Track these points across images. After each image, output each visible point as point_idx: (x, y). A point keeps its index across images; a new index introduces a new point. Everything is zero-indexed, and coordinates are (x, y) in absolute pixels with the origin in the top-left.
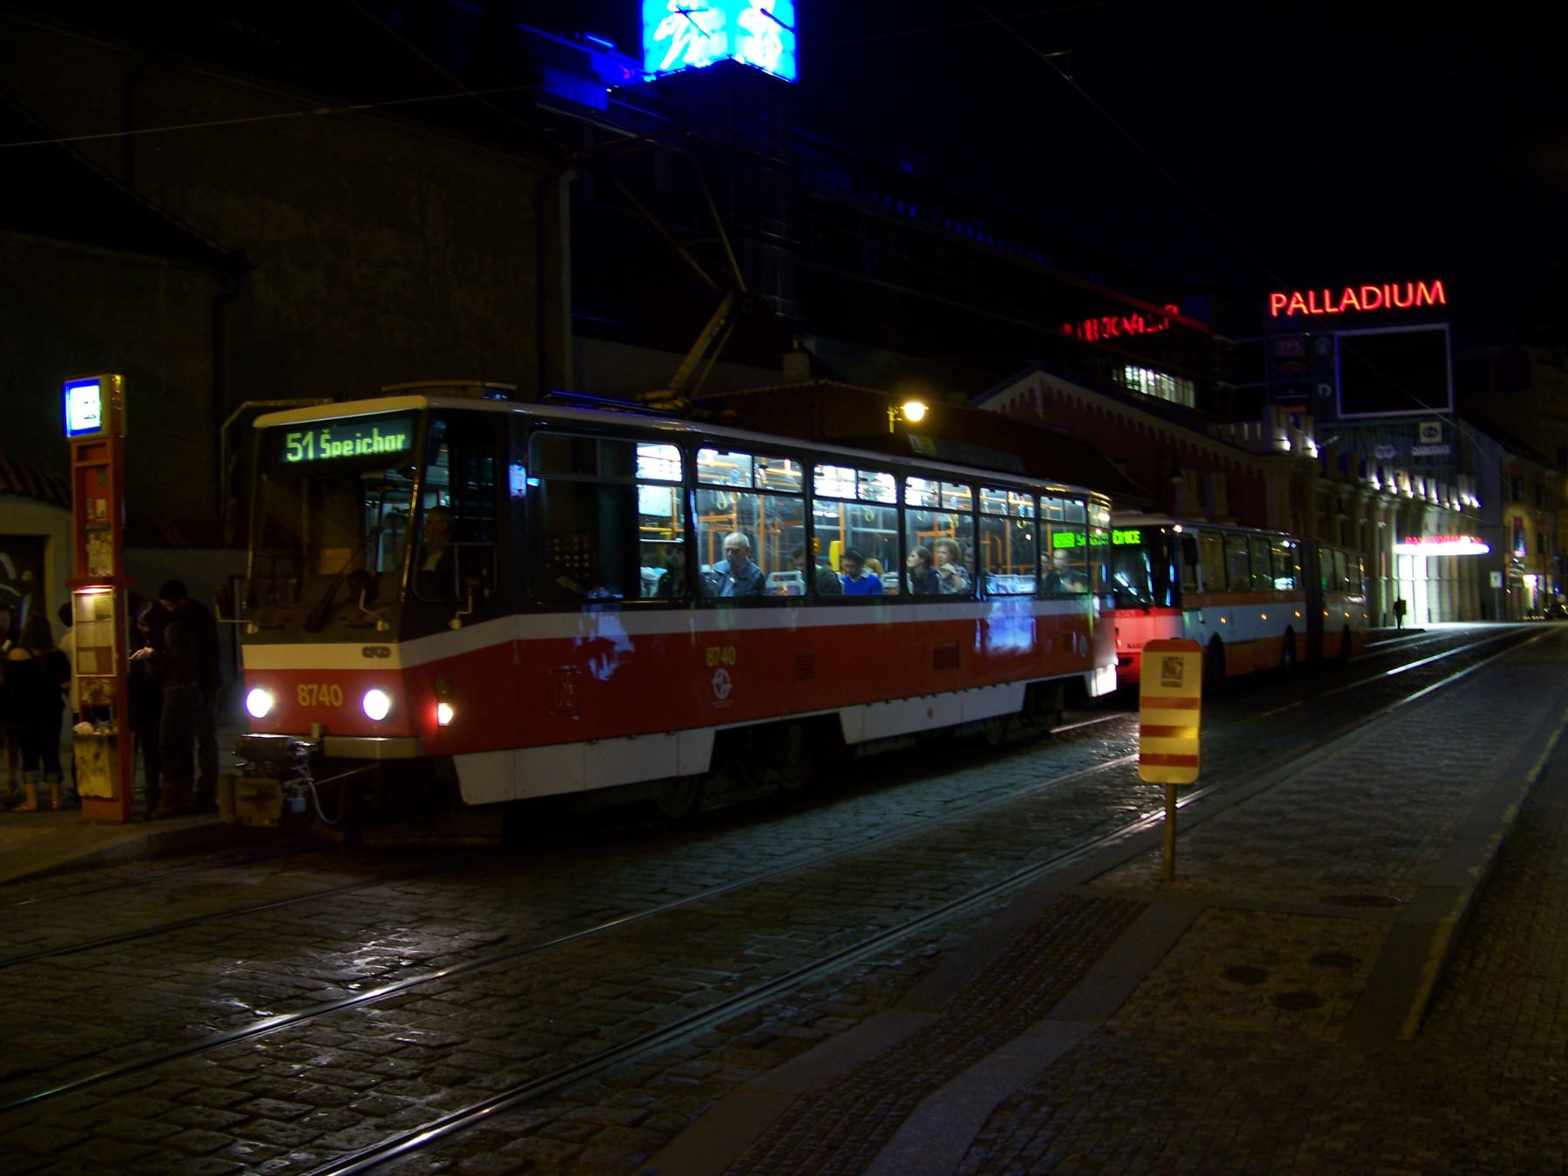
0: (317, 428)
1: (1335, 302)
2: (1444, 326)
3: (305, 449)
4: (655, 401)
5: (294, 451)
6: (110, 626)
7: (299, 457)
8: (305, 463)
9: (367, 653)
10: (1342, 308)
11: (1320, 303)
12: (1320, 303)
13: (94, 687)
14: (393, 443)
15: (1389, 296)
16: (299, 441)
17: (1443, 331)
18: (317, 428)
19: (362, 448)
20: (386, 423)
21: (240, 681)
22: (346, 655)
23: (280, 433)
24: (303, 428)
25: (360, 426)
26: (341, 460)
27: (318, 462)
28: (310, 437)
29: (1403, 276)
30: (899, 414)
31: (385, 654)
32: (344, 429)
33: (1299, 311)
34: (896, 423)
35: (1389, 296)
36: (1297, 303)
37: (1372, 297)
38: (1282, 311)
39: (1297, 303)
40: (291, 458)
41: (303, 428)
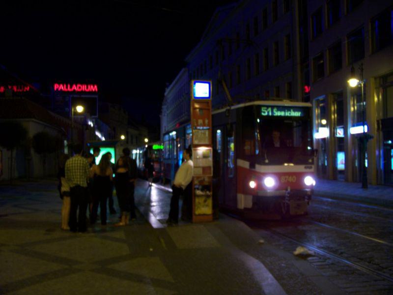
0: (273, 107)
1: (71, 87)
2: (97, 96)
3: (268, 112)
4: (334, 107)
5: (264, 112)
6: (211, 159)
7: (266, 114)
8: (268, 116)
9: (305, 168)
10: (72, 90)
11: (67, 88)
12: (67, 88)
13: (200, 179)
14: (298, 114)
15: (84, 88)
16: (266, 110)
17: (96, 98)
18: (273, 107)
19: (287, 114)
20: (296, 109)
21: (109, 177)
22: (301, 168)
23: (260, 107)
24: (268, 107)
25: (288, 108)
26: (280, 117)
27: (273, 117)
28: (270, 109)
29: (88, 83)
30: (75, 109)
31: (311, 168)
32: (280, 108)
33: (61, 90)
34: (74, 112)
35: (84, 88)
36: (62, 87)
37: (80, 88)
38: (57, 89)
39: (62, 87)
40: (263, 114)
41: (268, 107)
